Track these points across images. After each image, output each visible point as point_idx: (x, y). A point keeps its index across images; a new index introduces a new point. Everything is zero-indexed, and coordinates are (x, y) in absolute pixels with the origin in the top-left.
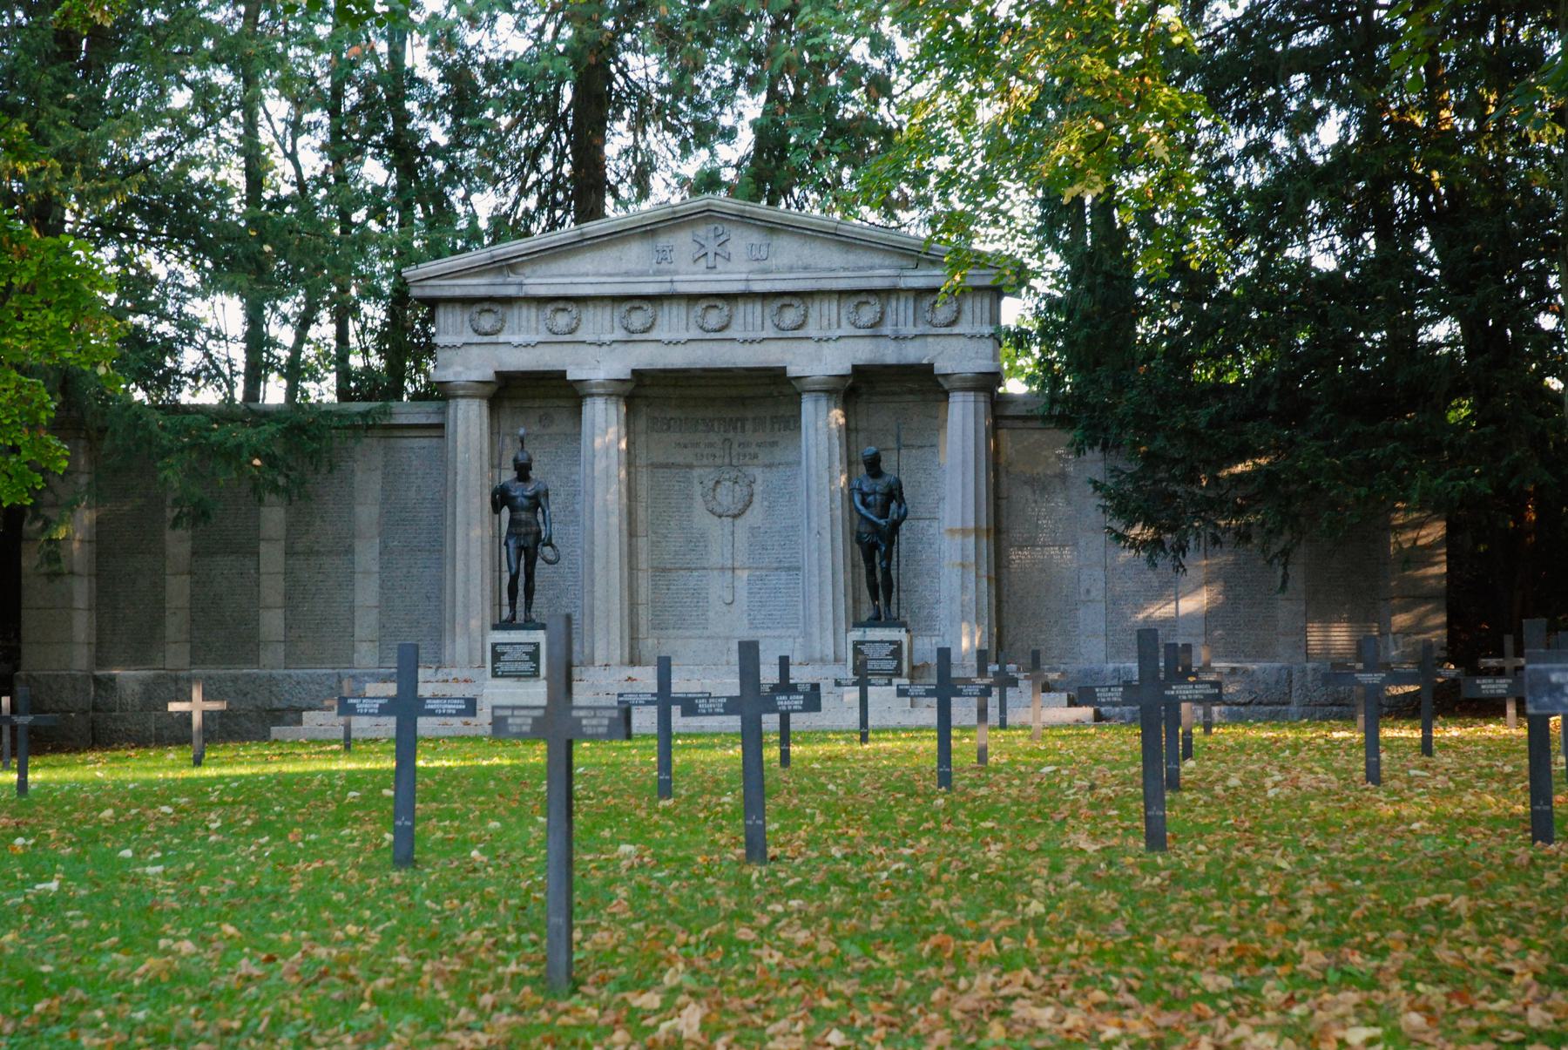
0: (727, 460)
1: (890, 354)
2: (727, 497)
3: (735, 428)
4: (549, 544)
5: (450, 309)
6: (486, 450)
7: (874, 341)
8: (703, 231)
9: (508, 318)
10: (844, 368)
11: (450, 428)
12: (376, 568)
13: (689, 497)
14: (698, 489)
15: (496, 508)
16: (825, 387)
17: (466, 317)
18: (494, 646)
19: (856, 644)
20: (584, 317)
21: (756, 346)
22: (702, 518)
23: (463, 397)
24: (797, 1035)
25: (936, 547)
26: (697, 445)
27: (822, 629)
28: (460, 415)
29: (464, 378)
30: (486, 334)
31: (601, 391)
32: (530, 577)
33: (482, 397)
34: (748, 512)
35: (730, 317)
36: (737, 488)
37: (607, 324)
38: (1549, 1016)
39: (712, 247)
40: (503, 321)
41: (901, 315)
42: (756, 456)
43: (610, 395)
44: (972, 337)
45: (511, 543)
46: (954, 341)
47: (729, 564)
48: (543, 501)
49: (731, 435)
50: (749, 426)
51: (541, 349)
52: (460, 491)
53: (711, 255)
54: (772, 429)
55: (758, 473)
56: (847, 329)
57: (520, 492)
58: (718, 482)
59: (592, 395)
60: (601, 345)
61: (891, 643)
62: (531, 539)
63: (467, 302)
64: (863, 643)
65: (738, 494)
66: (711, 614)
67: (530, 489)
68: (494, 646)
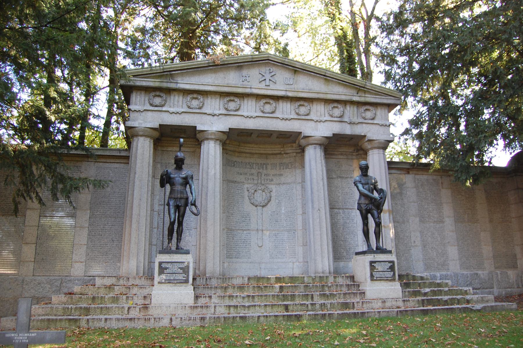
1: (348, 130)
2: (260, 197)
4: (194, 204)
5: (139, 93)
6: (151, 162)
7: (340, 123)
8: (264, 70)
9: (168, 100)
10: (329, 134)
11: (132, 159)
12: (87, 225)
13: (243, 197)
14: (246, 193)
15: (162, 185)
16: (319, 142)
17: (147, 99)
18: (160, 263)
19: (371, 263)
20: (205, 103)
21: (288, 122)
22: (248, 207)
23: (142, 136)
25: (355, 221)
27: (322, 257)
28: (139, 145)
29: (144, 125)
30: (156, 106)
31: (213, 137)
32: (180, 224)
33: (150, 137)
34: (269, 205)
35: (276, 107)
37: (217, 107)
39: (268, 77)
40: (166, 101)
41: (350, 112)
42: (272, 180)
43: (217, 140)
44: (382, 125)
45: (172, 203)
46: (374, 126)
47: (260, 228)
48: (190, 182)
49: (261, 171)
50: (269, 167)
51: (183, 115)
52: (137, 183)
53: (267, 80)
54: (280, 169)
55: (273, 187)
56: (328, 118)
57: (178, 177)
58: (255, 191)
59: (207, 139)
60: (214, 115)
61: (390, 262)
62: (183, 202)
63: (147, 90)
64: (375, 262)
65: (264, 197)
66: (252, 251)
67: (183, 174)
68: (160, 263)
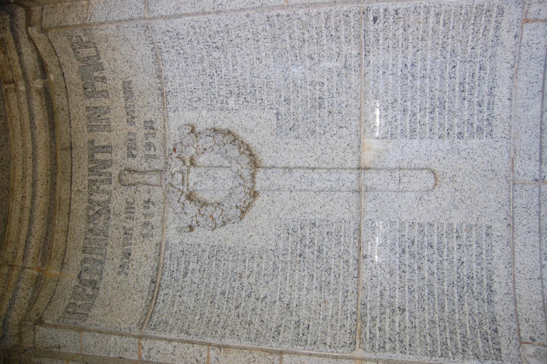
0: (154, 179)
3: (106, 164)
24: (164, 207)
26: (127, 233)
34: (249, 139)
36: (201, 160)
38: (376, 312)
42: (149, 125)
50: (101, 138)
54: (105, 93)
58: (190, 197)
65: (216, 159)
